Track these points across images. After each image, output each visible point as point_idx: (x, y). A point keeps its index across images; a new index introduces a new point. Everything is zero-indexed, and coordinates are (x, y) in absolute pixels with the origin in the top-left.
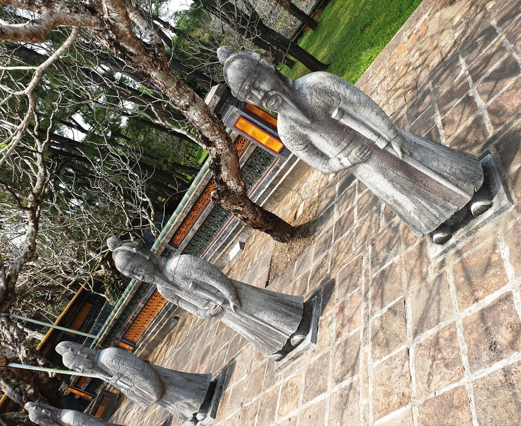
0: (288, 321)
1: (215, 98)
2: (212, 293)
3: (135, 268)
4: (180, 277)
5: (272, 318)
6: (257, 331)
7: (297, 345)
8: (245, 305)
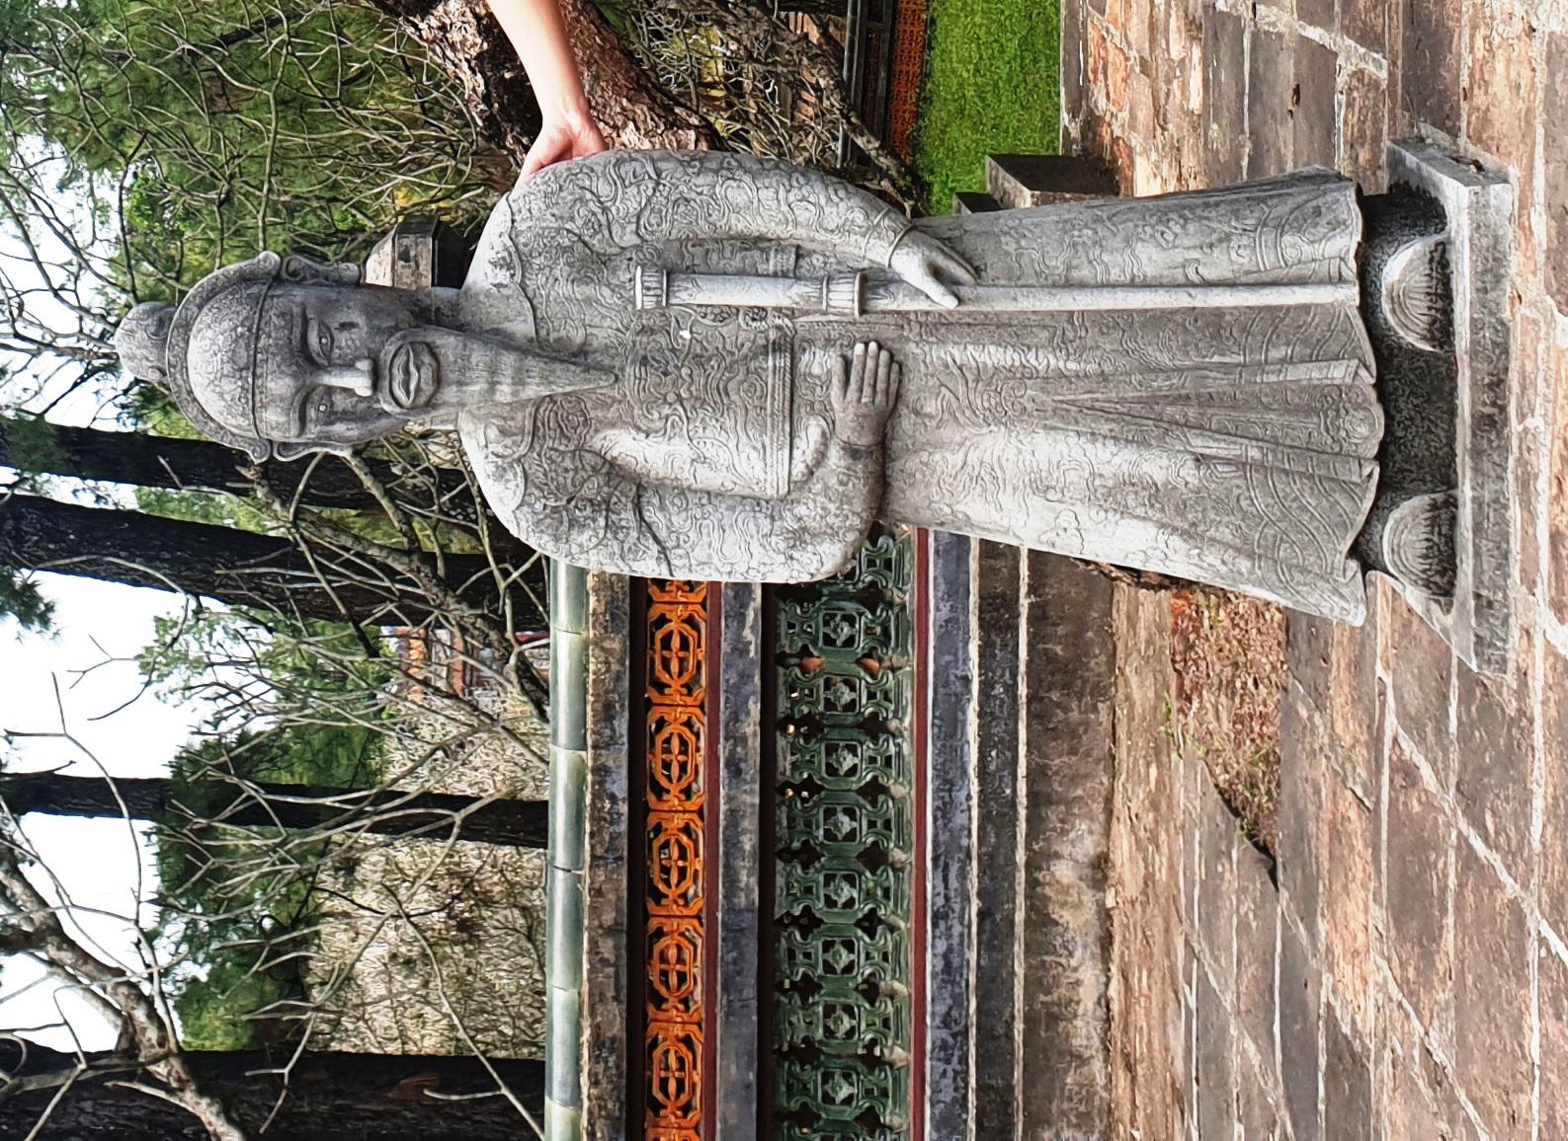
0: (1283, 209)
1: (404, 256)
2: (775, 275)
3: (305, 321)
4: (561, 270)
5: (1186, 242)
6: (1159, 382)
7: (1442, 328)
8: (991, 259)
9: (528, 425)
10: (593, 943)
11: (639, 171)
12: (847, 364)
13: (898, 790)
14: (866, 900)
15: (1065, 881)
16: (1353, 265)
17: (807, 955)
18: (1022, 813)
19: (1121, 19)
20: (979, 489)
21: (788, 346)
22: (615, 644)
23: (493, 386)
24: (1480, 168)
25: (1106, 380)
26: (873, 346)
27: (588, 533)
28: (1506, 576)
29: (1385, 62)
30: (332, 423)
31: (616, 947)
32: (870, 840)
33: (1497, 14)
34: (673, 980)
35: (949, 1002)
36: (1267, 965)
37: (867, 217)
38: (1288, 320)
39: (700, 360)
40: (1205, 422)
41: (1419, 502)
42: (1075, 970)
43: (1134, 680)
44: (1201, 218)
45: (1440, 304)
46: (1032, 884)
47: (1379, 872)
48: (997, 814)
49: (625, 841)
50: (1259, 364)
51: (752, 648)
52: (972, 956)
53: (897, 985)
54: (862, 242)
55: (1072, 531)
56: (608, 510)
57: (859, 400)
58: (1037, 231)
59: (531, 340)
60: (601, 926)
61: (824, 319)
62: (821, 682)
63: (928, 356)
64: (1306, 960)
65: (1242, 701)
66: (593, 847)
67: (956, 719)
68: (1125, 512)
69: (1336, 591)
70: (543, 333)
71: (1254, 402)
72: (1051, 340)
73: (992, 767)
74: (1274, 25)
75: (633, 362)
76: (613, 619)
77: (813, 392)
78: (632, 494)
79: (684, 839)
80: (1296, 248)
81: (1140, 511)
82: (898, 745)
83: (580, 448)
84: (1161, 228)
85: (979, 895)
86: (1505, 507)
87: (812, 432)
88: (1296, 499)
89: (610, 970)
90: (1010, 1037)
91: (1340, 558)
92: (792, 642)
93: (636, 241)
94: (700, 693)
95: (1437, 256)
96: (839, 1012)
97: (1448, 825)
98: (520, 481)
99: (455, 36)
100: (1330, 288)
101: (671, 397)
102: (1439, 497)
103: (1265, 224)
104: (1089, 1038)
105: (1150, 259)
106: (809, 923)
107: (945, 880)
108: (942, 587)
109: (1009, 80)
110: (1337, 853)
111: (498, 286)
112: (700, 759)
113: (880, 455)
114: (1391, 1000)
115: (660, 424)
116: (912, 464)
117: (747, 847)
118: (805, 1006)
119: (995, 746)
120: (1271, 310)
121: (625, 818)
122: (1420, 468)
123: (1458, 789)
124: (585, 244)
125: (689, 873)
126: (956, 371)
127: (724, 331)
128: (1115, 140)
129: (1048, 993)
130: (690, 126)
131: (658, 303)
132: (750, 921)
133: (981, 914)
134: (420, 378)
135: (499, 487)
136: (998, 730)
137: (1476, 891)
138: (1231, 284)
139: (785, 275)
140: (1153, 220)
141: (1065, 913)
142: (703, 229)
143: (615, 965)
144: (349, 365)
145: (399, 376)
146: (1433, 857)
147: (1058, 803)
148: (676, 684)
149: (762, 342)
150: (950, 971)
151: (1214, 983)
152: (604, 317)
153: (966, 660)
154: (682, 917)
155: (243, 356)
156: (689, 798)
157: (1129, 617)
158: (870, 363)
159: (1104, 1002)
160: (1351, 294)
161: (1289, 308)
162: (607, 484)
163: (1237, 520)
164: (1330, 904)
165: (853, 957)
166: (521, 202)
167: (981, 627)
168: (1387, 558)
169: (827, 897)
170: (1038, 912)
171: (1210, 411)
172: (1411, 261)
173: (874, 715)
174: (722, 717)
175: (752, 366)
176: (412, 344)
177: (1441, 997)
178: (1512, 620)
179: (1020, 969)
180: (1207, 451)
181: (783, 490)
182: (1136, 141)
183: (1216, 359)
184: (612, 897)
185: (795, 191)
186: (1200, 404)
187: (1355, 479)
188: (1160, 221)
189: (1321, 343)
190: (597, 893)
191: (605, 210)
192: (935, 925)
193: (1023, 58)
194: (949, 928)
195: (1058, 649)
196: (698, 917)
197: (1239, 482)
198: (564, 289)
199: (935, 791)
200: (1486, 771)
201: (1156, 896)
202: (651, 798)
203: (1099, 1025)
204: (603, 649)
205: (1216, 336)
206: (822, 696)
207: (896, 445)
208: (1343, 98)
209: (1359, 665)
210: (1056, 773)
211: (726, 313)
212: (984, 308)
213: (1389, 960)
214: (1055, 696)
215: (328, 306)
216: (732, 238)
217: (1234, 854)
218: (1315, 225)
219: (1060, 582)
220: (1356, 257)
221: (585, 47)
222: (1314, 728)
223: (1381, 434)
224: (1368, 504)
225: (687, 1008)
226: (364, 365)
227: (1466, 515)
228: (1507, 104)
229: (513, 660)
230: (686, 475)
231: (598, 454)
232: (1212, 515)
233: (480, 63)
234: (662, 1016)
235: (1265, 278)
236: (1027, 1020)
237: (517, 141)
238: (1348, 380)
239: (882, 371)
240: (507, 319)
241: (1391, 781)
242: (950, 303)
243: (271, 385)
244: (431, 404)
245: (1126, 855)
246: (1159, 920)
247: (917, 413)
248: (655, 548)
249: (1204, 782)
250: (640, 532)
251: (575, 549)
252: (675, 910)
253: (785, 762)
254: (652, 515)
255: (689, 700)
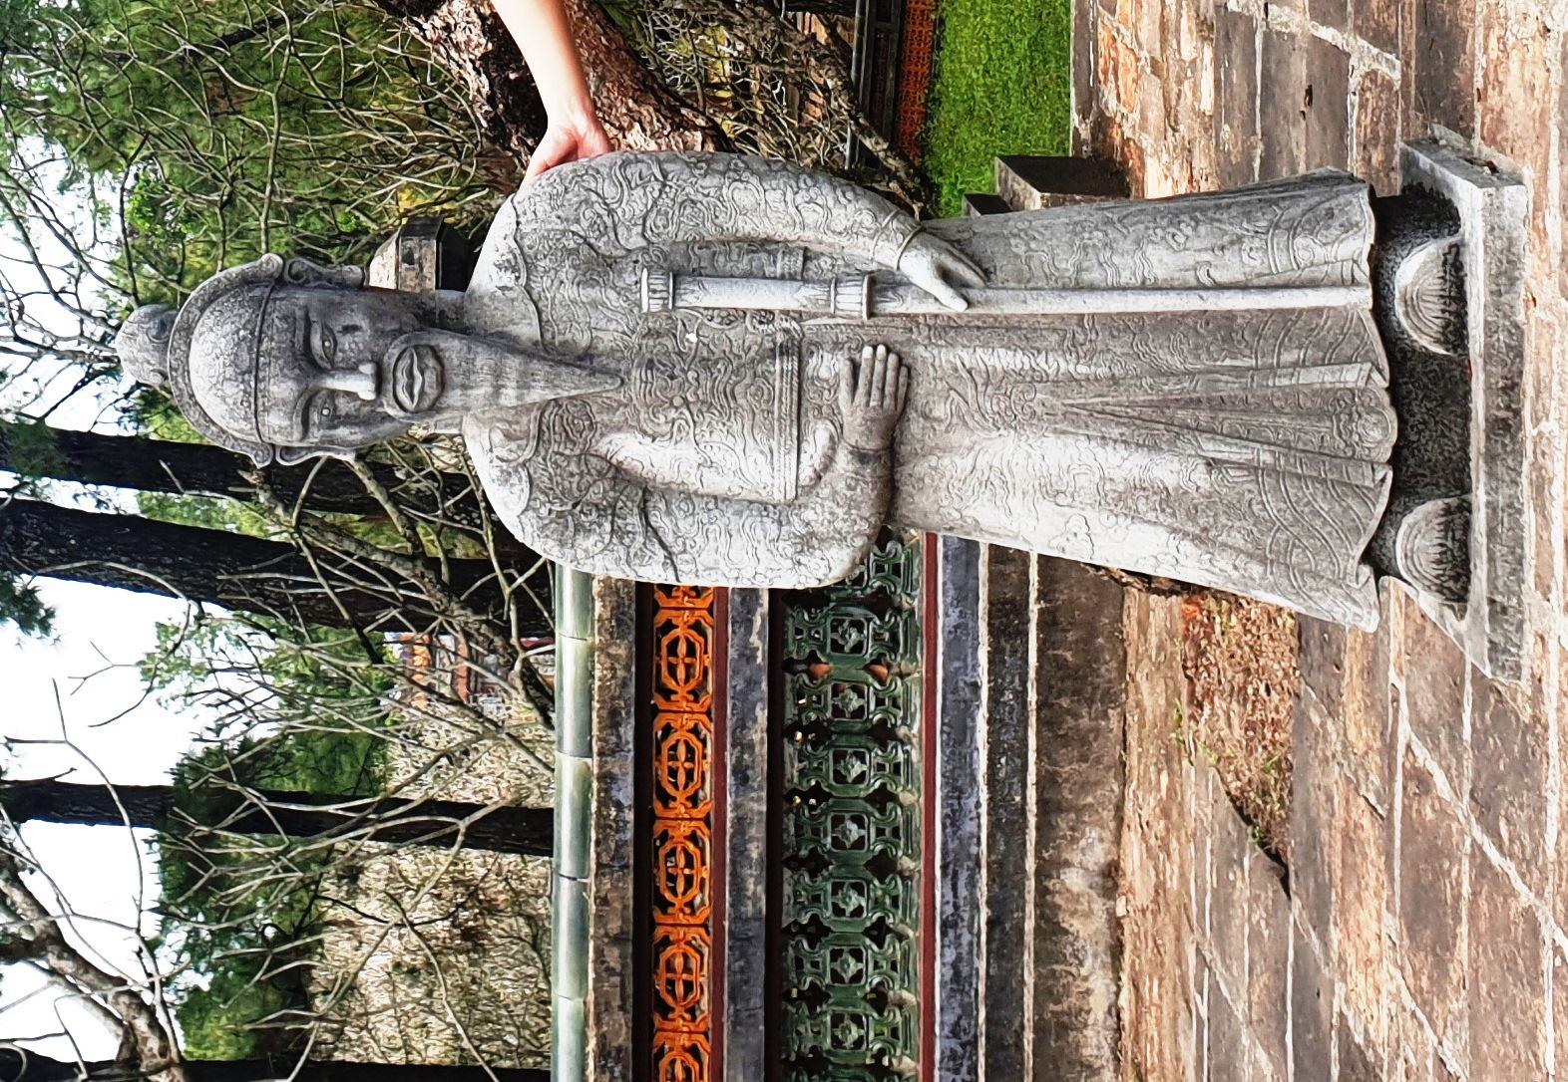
0: (1295, 211)
1: (408, 258)
2: (782, 277)
3: (308, 324)
4: (567, 272)
5: (1197, 244)
6: (1170, 386)
7: (1455, 331)
8: (1000, 262)
9: (534, 430)
10: (599, 952)
11: (645, 172)
12: (855, 368)
13: (906, 798)
14: (874, 909)
15: (1075, 889)
16: (1366, 267)
17: (815, 964)
18: (1032, 820)
19: (1132, 19)
20: (988, 493)
21: (796, 349)
22: (621, 650)
23: (497, 389)
24: (1494, 169)
25: (1116, 383)
26: (881, 349)
27: (594, 538)
28: (1521, 581)
29: (1398, 63)
30: (335, 427)
31: (622, 956)
32: (879, 848)
33: (1511, 14)
34: (680, 989)
35: (958, 1011)
36: (1279, 974)
37: (876, 218)
38: (1300, 323)
39: (707, 364)
40: (1217, 426)
41: (1433, 507)
42: (1085, 979)
43: (1145, 687)
44: (1212, 220)
45: (1453, 307)
46: (1042, 892)
47: (1392, 880)
48: (1006, 822)
49: (631, 849)
50: (1271, 367)
51: (759, 654)
52: (982, 965)
53: (905, 995)
54: (870, 244)
55: (1082, 536)
56: (614, 515)
57: (867, 404)
58: (1047, 233)
59: (536, 343)
60: (606, 935)
61: (832, 322)
62: (829, 688)
63: (935, 359)
64: (1318, 969)
65: (1254, 708)
66: (598, 855)
67: (965, 727)
68: (1135, 516)
69: (1348, 597)
70: (548, 336)
71: (1267, 406)
72: (1061, 343)
73: (1002, 774)
74: (1287, 25)
75: (639, 366)
76: (618, 620)
77: (821, 396)
78: (638, 499)
79: (691, 847)
80: (1309, 250)
81: (1151, 516)
82: (906, 752)
83: (585, 453)
84: (1172, 230)
85: (989, 903)
86: (1520, 512)
87: (819, 435)
88: (1308, 503)
89: (616, 980)
90: (1019, 1047)
91: (1353, 563)
92: (799, 648)
93: (643, 243)
94: (706, 700)
95: (1450, 258)
96: (847, 1021)
97: (1462, 832)
98: (525, 485)
99: (459, 36)
100: (1343, 291)
101: (677, 401)
102: (1453, 501)
103: (1277, 226)
104: (1099, 1048)
105: (1161, 261)
106: (817, 932)
107: (954, 888)
108: (951, 593)
109: (1019, 81)
110: (1350, 860)
111: (503, 288)
112: (707, 766)
113: (888, 459)
114: (1404, 1009)
115: (666, 428)
116: (921, 468)
117: (755, 855)
118: (813, 1015)
119: (1004, 753)
120: (1283, 313)
121: (630, 826)
122: (1433, 472)
123: (1472, 796)
124: (591, 246)
125: (696, 882)
126: (965, 375)
127: (731, 334)
128: (1126, 141)
129: (1058, 1002)
130: (696, 128)
131: (665, 305)
132: (757, 929)
133: (989, 922)
134: (425, 381)
135: (504, 491)
136: (1008, 737)
137: (1490, 899)
138: (1243, 287)
139: (792, 278)
140: (1164, 223)
141: (1075, 922)
142: (710, 231)
143: (620, 974)
144: (352, 369)
145: (403, 379)
146: (1446, 865)
147: (1068, 811)
148: (682, 691)
149: (769, 345)
150: (959, 980)
151: (1225, 993)
152: (610, 320)
153: (975, 666)
154: (689, 926)
155: (245, 359)
156: (695, 805)
157: (1140, 623)
158: (879, 367)
159: (1115, 1011)
160: (1364, 297)
161: (1301, 311)
162: (613, 489)
163: (1248, 524)
164: (1343, 912)
165: (861, 966)
166: (526, 204)
167: (990, 633)
168: (1400, 563)
169: (835, 906)
170: (1048, 921)
171: (1222, 415)
172: (1425, 263)
173: (883, 722)
174: (729, 724)
175: (759, 369)
176: (416, 347)
177: (1455, 1006)
178: (1526, 626)
179: (1029, 978)
180: (1219, 456)
181: (791, 495)
182: (1147, 142)
183: (1228, 362)
184: (618, 905)
185: (802, 193)
186: (1211, 408)
187: (1368, 483)
188: (1171, 223)
189: (1334, 346)
190: (603, 901)
191: (611, 212)
192: (944, 934)
193: (1033, 59)
194: (958, 937)
195: (1068, 655)
196: (705, 926)
197: (1250, 486)
198: (569, 292)
199: (945, 798)
200: (1500, 779)
201: (1167, 905)
202: (658, 806)
203: (1110, 1034)
204: (609, 655)
205: (1228, 339)
206: (830, 702)
207: (905, 450)
208: (1356, 99)
209: (1372, 672)
210: (1066, 780)
211: (733, 317)
212: (994, 311)
213: (1402, 969)
214: (1065, 702)
215: (332, 309)
216: (739, 240)
217: (1246, 862)
218: (1328, 227)
219: (1070, 588)
220: (1369, 259)
221: (591, 48)
222: (1326, 735)
223: (1394, 438)
224: (1381, 509)
225: (694, 1018)
226: (367, 369)
227: (1480, 520)
228: (1521, 105)
229: (518, 666)
230: (693, 479)
231: (604, 458)
232: (1223, 519)
233: (485, 64)
234: (668, 1025)
235: (1277, 280)
236: (1036, 1030)
237: (522, 142)
238: (1361, 384)
239: (890, 374)
240: (512, 322)
241: (1405, 788)
242: (958, 306)
243: (273, 388)
244: (435, 408)
245: (1137, 863)
246: (1170, 929)
247: (926, 417)
248: (661, 553)
249: (1216, 789)
250: (646, 537)
251: (580, 554)
252: (682, 918)
253: (793, 769)
254: (658, 519)
255: (696, 707)
